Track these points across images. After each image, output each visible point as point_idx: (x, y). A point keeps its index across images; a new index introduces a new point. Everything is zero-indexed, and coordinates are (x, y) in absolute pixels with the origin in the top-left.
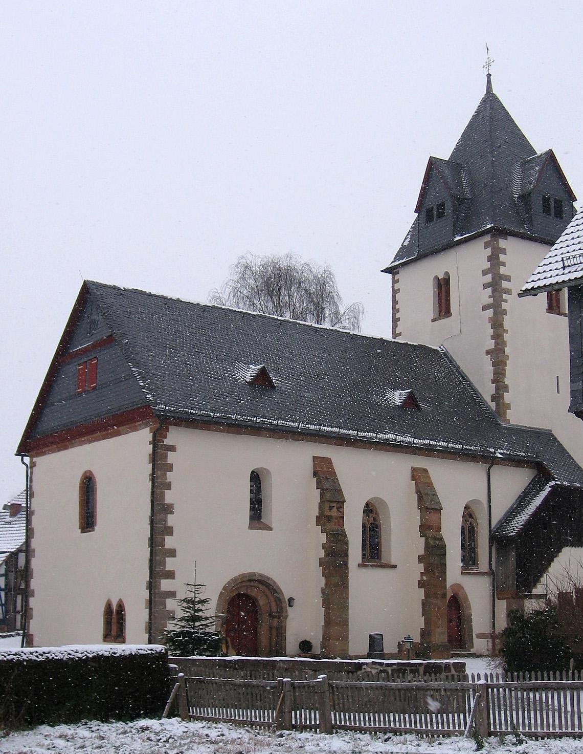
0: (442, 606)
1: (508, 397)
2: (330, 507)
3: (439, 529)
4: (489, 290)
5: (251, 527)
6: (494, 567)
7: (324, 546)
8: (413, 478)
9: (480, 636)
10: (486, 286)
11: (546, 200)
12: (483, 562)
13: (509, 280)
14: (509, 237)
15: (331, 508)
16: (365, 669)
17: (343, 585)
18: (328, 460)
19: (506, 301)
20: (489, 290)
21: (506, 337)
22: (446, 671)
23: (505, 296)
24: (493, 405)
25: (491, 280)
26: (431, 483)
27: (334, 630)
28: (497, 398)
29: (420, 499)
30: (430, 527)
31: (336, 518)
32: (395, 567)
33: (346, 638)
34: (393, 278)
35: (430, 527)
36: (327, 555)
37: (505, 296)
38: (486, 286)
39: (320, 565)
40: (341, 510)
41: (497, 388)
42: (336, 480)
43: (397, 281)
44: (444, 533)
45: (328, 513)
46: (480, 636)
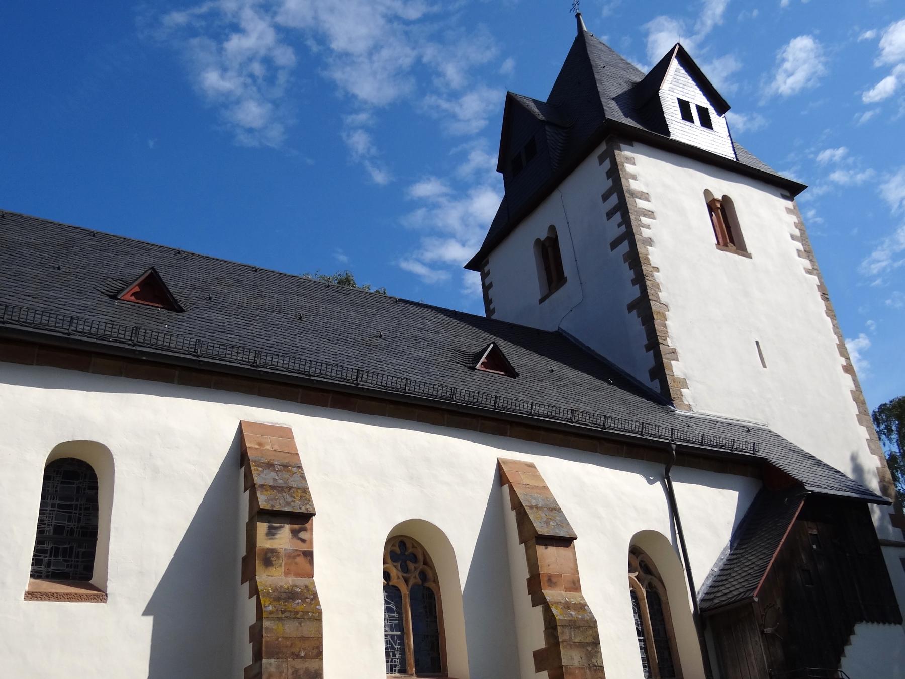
3: (575, 586)
4: (618, 217)
11: (684, 106)
14: (635, 144)
19: (648, 227)
20: (618, 217)
31: (292, 556)
37: (644, 220)
38: (610, 215)
40: (302, 535)
42: (294, 470)
43: (488, 273)
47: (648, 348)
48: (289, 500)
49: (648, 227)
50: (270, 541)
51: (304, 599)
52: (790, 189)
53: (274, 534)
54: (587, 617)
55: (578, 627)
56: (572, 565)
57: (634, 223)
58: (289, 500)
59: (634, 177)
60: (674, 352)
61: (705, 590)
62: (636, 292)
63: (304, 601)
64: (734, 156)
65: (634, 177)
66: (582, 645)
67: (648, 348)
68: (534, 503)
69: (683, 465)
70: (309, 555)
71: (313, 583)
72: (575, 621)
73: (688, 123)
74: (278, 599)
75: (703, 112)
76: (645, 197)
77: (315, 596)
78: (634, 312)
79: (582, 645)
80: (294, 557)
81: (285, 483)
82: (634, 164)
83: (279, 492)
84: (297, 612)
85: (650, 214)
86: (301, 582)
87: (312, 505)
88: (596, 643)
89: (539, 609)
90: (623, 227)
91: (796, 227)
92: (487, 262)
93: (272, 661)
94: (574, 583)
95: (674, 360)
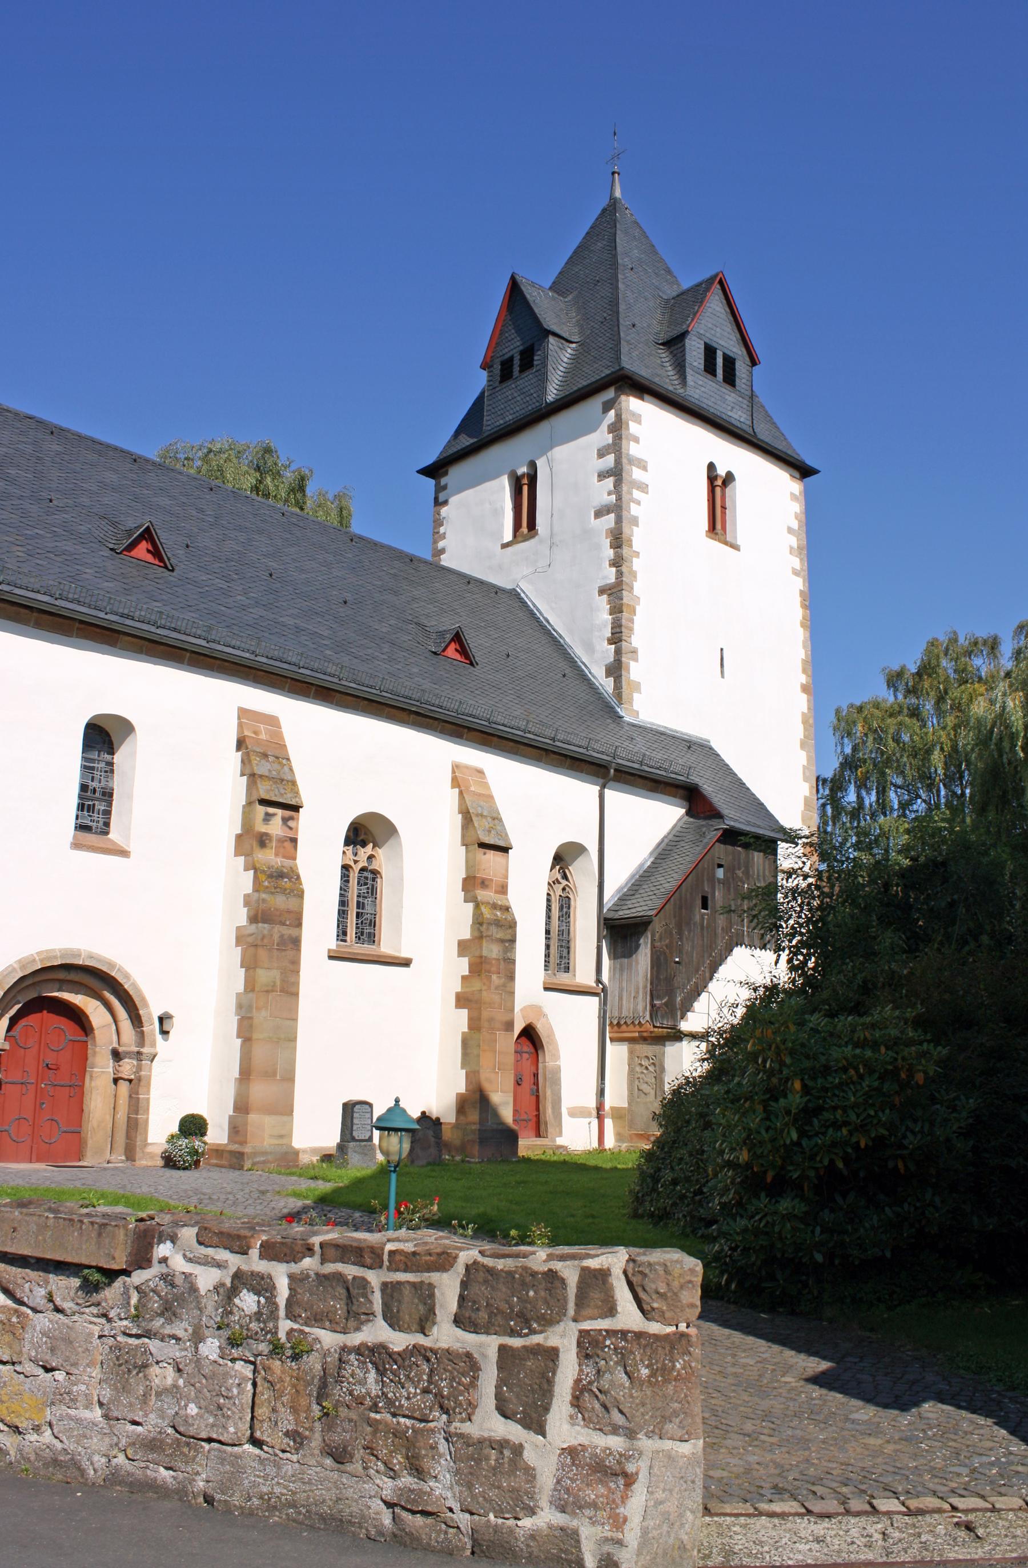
0: (507, 1043)
1: (635, 671)
2: (267, 814)
3: (503, 889)
4: (610, 482)
5: (76, 845)
6: (605, 977)
7: (247, 902)
8: (455, 782)
9: (574, 1113)
10: (602, 476)
11: (710, 352)
12: (584, 973)
13: (645, 468)
14: (646, 397)
15: (268, 817)
16: (164, 1260)
17: (289, 989)
18: (272, 721)
19: (639, 503)
20: (610, 482)
21: (637, 564)
22: (586, 1312)
23: (636, 494)
24: (607, 685)
25: (612, 465)
26: (491, 797)
27: (259, 1091)
28: (616, 670)
29: (467, 818)
30: (484, 884)
31: (281, 841)
32: (406, 963)
33: (288, 1110)
34: (437, 485)
35: (484, 884)
36: (253, 919)
37: (636, 494)
38: (602, 476)
39: (238, 944)
40: (291, 823)
41: (618, 652)
42: (284, 762)
43: (445, 488)
44: (515, 898)
45: (261, 828)
46: (574, 1113)
47: (611, 642)
48: (283, 791)
49: (639, 503)
50: (266, 826)
51: (290, 878)
52: (803, 471)
53: (269, 820)
54: (509, 918)
55: (501, 926)
56: (504, 872)
57: (625, 497)
58: (283, 791)
59: (637, 440)
60: (634, 652)
61: (610, 905)
62: (610, 575)
63: (290, 880)
64: (749, 423)
65: (637, 440)
66: (502, 941)
67: (611, 642)
68: (480, 811)
69: (619, 782)
70: (294, 841)
71: (296, 865)
72: (499, 921)
73: (709, 376)
74: (271, 876)
75: (730, 362)
76: (643, 466)
77: (298, 877)
78: (605, 597)
79: (502, 941)
80: (283, 842)
81: (278, 774)
82: (639, 423)
83: (275, 783)
84: (285, 889)
85: (643, 488)
86: (288, 862)
87: (300, 798)
88: (513, 941)
89: (471, 906)
90: (613, 497)
91: (796, 518)
92: (446, 473)
93: (266, 925)
94: (503, 887)
95: (635, 421)
